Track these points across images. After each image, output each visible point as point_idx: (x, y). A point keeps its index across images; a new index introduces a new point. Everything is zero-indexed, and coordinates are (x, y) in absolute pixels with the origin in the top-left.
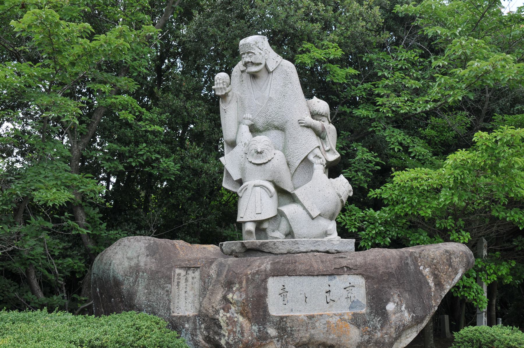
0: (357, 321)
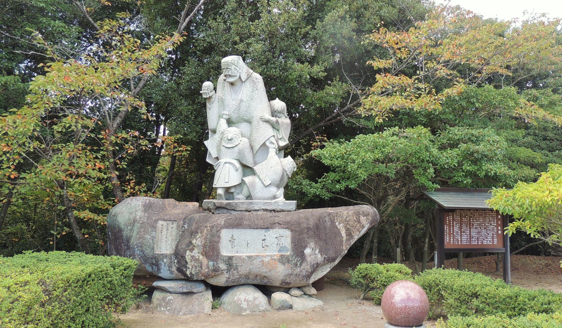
0: (283, 260)
